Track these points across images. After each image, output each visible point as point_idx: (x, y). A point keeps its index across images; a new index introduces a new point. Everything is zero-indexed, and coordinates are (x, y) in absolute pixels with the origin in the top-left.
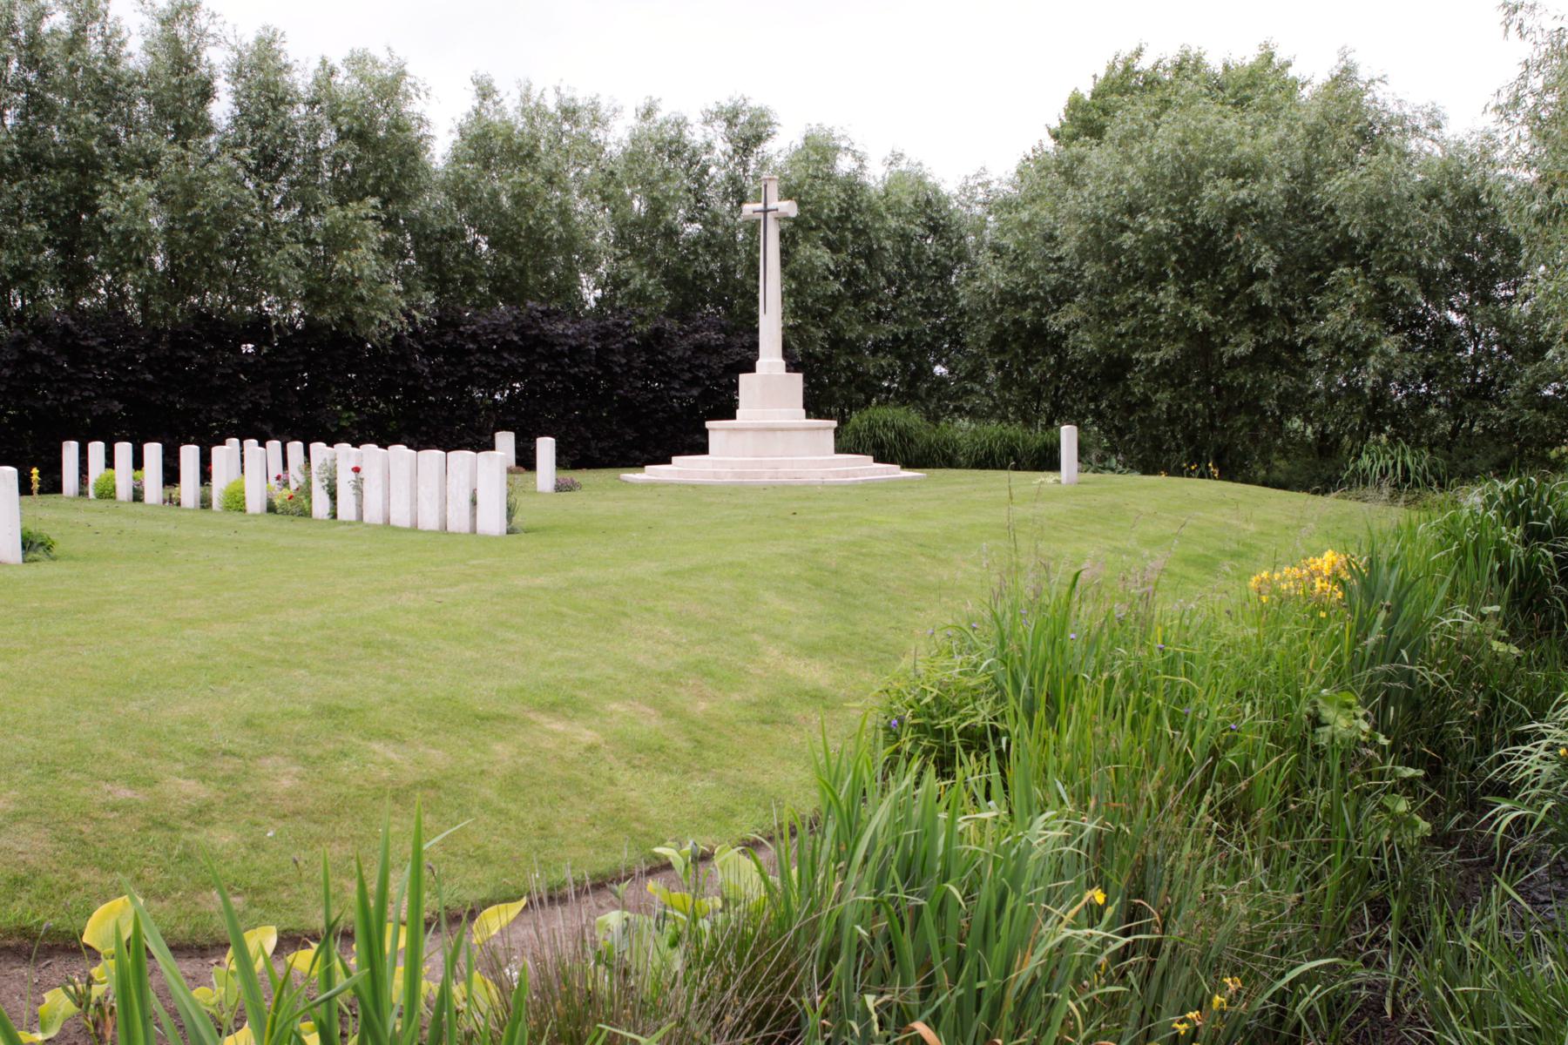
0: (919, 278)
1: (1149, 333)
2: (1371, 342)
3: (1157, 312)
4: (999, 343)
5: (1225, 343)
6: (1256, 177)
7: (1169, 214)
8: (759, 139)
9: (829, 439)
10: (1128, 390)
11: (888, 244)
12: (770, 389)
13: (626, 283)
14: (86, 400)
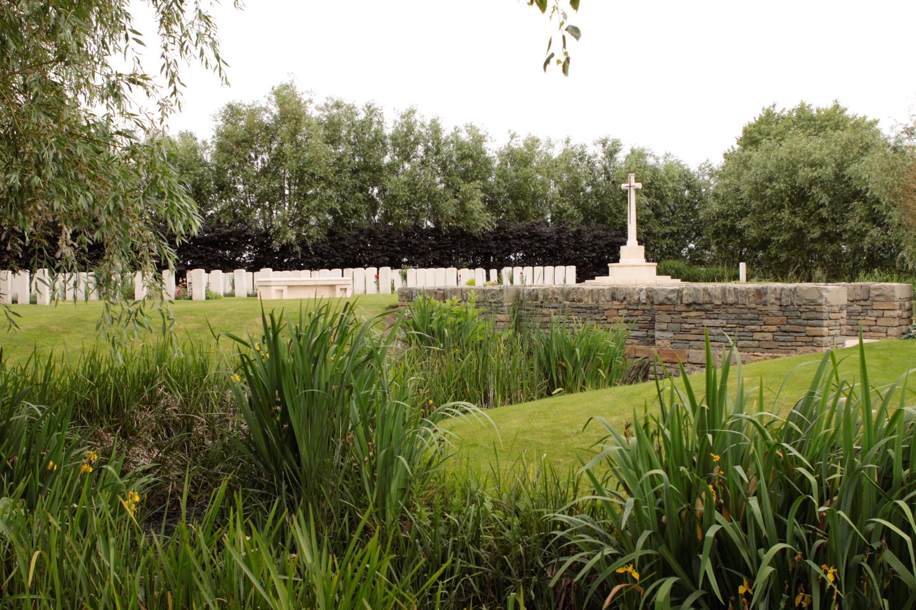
0: (682, 207)
1: (777, 229)
2: (867, 231)
3: (781, 221)
4: (716, 234)
5: (809, 232)
6: (821, 167)
7: (785, 182)
8: (616, 151)
9: (654, 270)
10: (769, 253)
11: (669, 194)
12: (632, 252)
13: (566, 211)
14: (378, 257)
